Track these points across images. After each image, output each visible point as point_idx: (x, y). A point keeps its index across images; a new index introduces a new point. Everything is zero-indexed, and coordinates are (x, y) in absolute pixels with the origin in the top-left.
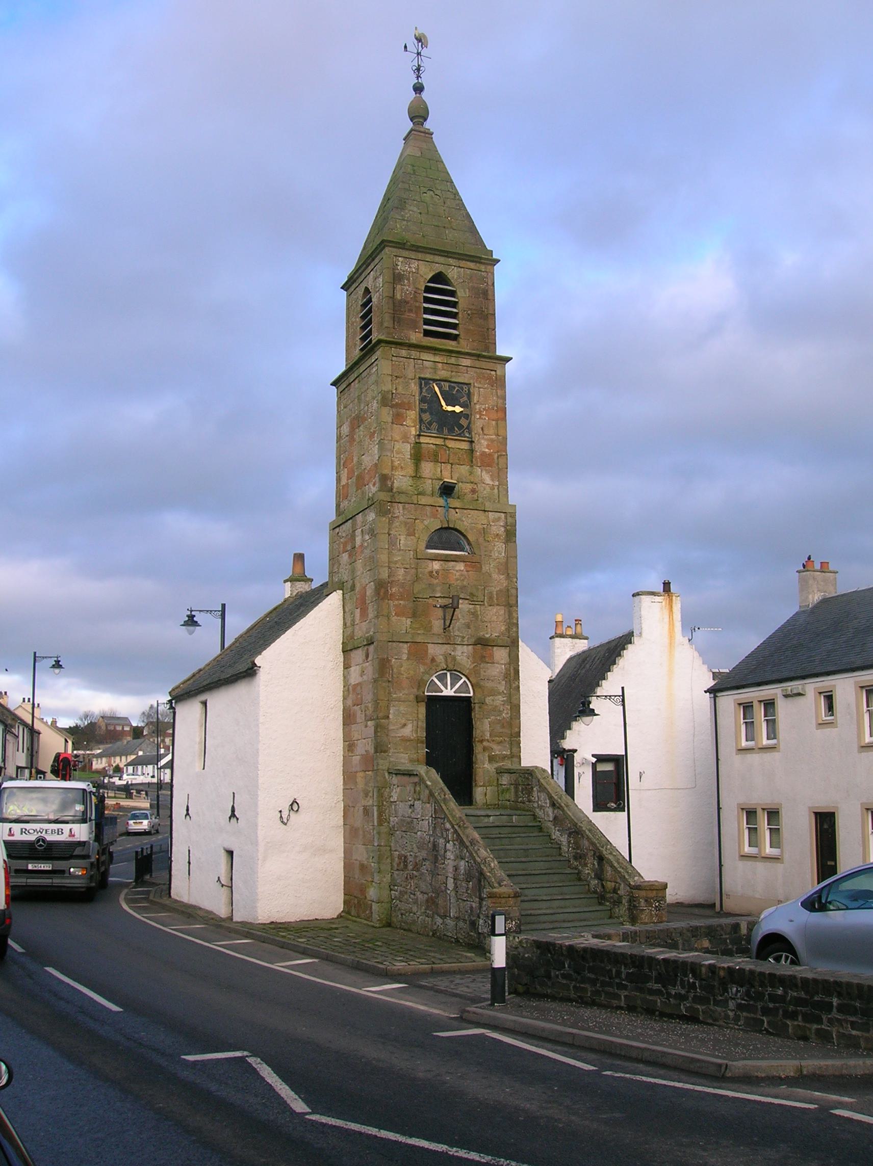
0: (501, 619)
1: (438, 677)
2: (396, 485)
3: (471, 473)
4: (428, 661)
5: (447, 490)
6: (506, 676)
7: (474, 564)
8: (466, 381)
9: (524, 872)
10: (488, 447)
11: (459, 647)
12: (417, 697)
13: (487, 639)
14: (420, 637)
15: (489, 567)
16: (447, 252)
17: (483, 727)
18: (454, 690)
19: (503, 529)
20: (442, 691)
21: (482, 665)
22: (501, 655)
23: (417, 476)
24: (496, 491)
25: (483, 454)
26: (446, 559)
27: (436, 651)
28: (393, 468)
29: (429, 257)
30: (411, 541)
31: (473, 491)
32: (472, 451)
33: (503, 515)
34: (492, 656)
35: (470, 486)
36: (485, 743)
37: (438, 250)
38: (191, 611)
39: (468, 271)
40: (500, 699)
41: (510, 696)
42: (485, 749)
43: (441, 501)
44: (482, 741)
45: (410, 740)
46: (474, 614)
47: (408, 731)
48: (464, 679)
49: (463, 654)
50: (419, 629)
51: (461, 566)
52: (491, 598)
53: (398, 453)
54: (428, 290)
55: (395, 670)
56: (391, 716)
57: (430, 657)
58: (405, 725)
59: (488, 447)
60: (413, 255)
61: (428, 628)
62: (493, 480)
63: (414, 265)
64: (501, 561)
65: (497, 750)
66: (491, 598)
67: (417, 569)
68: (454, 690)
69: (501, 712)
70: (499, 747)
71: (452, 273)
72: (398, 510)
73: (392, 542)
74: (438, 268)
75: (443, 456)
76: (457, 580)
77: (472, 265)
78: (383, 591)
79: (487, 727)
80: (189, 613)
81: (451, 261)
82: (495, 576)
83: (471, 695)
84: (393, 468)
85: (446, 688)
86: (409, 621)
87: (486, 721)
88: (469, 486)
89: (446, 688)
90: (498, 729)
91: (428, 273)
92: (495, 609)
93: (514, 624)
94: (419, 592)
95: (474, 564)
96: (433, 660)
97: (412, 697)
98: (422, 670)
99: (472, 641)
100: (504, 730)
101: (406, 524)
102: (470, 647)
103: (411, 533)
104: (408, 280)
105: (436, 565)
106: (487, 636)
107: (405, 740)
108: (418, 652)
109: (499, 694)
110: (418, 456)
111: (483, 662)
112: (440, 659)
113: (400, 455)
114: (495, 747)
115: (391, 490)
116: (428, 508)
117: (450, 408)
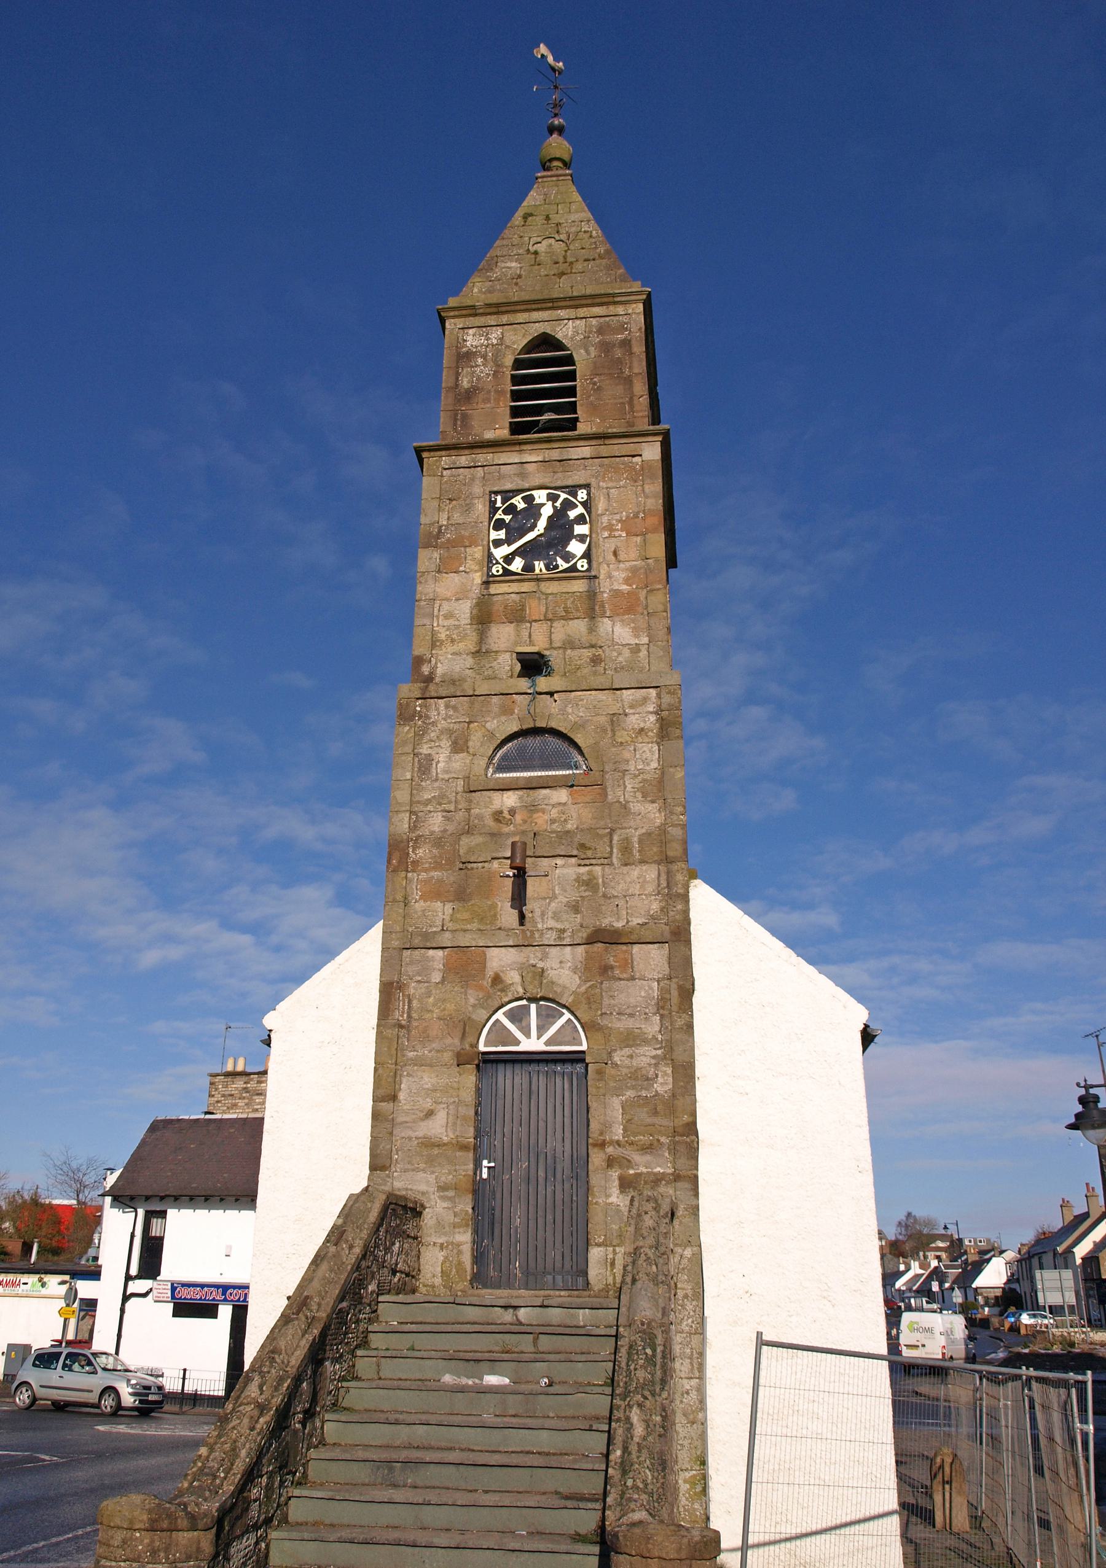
0: (650, 888)
1: (513, 1016)
2: (440, 670)
3: (591, 630)
4: (487, 983)
5: (533, 666)
6: (662, 1005)
7: (593, 785)
8: (582, 482)
9: (394, 1535)
10: (627, 581)
11: (554, 951)
12: (458, 1055)
13: (617, 932)
14: (468, 936)
15: (626, 791)
16: (552, 300)
17: (611, 1114)
18: (545, 1037)
19: (653, 718)
20: (518, 1043)
21: (606, 984)
22: (652, 960)
23: (481, 653)
24: (643, 653)
25: (616, 593)
26: (531, 786)
27: (502, 960)
28: (435, 643)
29: (521, 317)
30: (460, 762)
31: (596, 661)
32: (592, 595)
33: (653, 692)
34: (628, 964)
35: (587, 653)
36: (610, 1150)
37: (535, 302)
38: (1087, 1087)
39: (594, 321)
40: (645, 1056)
41: (669, 1047)
42: (611, 1162)
43: (524, 684)
44: (602, 1145)
45: (440, 1145)
46: (589, 883)
47: (438, 1127)
48: (567, 1015)
49: (564, 969)
50: (470, 921)
51: (562, 795)
52: (626, 849)
53: (446, 617)
54: (518, 364)
55: (415, 1003)
56: (402, 1096)
57: (490, 973)
58: (430, 1114)
59: (627, 581)
60: (491, 320)
61: (487, 918)
62: (637, 636)
63: (495, 335)
64: (647, 777)
65: (642, 1164)
66: (626, 849)
67: (468, 810)
68: (545, 1037)
69: (650, 1080)
70: (648, 1157)
71: (569, 330)
72: (439, 711)
73: (425, 766)
74: (536, 330)
75: (535, 608)
76: (553, 821)
77: (597, 310)
78: (396, 855)
79: (616, 1103)
80: (1082, 1092)
81: (562, 313)
82: (635, 807)
83: (584, 1047)
84: (435, 643)
85: (527, 1034)
86: (449, 907)
87: (616, 1103)
88: (587, 653)
89: (527, 1034)
90: (643, 1115)
91: (518, 339)
92: (635, 872)
93: (678, 895)
94: (470, 850)
95: (593, 785)
96: (497, 979)
97: (448, 1057)
98: (472, 1001)
99: (583, 935)
100: (657, 1120)
101: (450, 732)
102: (581, 950)
103: (459, 746)
104: (484, 357)
105: (510, 799)
106: (619, 925)
107: (428, 1143)
108: (465, 966)
109: (646, 1042)
110: (483, 618)
111: (609, 979)
112: (513, 977)
113: (451, 622)
114: (637, 1157)
115: (429, 679)
116: (495, 699)
117: (542, 524)
